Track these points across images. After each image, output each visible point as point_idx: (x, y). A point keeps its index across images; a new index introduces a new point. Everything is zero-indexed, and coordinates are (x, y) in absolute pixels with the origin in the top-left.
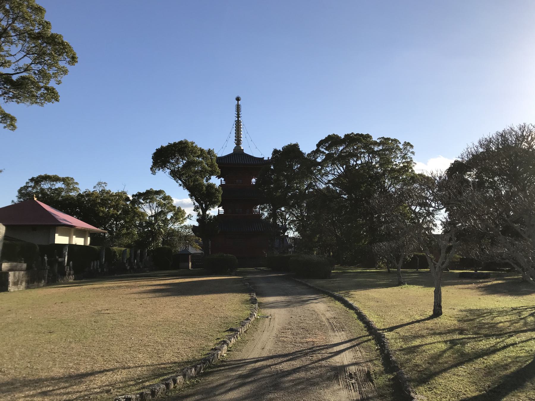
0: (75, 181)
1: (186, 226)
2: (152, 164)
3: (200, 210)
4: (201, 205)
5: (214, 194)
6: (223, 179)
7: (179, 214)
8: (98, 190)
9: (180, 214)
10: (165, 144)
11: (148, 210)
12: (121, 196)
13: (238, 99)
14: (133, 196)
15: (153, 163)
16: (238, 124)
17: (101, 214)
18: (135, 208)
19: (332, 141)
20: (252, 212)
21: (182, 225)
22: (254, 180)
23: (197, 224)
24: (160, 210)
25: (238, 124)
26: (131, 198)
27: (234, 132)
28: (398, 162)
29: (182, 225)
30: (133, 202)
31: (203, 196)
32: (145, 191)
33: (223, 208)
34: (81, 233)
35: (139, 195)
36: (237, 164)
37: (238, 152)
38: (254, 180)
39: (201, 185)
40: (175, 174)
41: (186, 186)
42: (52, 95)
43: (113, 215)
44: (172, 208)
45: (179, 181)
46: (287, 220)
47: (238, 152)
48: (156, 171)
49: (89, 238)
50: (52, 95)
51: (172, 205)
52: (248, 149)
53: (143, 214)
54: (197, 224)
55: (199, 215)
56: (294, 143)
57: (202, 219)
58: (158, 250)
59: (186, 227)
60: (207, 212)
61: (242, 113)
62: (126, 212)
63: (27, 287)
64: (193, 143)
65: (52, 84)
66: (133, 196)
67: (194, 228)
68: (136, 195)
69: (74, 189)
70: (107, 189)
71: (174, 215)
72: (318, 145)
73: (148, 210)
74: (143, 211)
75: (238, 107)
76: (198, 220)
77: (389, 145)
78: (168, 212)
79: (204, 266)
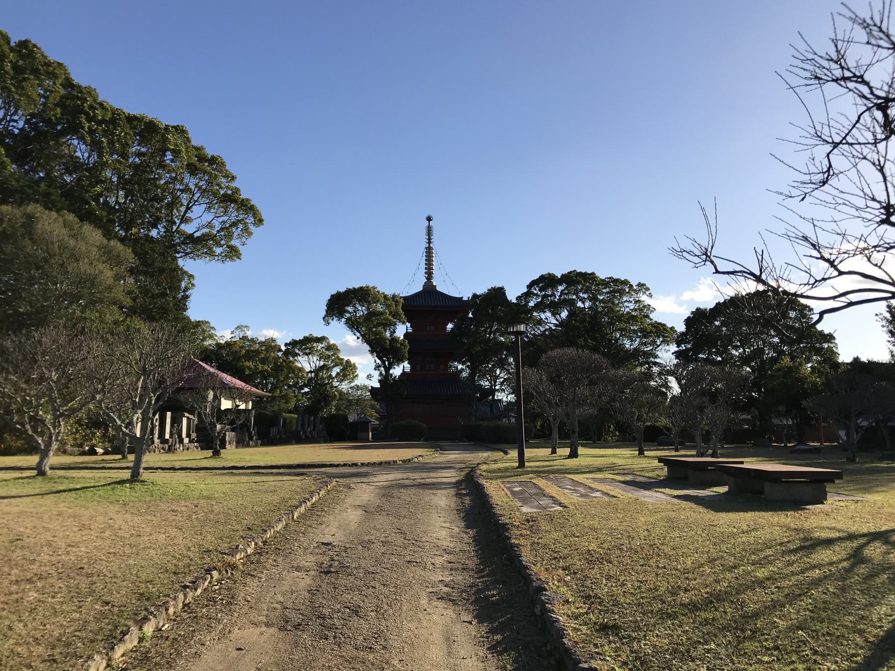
0: (211, 325)
1: (358, 386)
2: (325, 313)
3: (382, 369)
4: (383, 362)
5: (399, 349)
6: (408, 325)
7: (348, 370)
8: (238, 335)
9: (349, 369)
10: (342, 290)
11: (306, 363)
12: (270, 345)
13: (429, 219)
14: (286, 345)
15: (327, 311)
16: (429, 252)
17: (247, 372)
18: (291, 362)
19: (547, 281)
20: (447, 367)
21: (353, 384)
22: (450, 326)
23: (377, 385)
24: (322, 363)
25: (429, 252)
26: (283, 348)
27: (423, 266)
28: (628, 306)
29: (353, 384)
30: (287, 353)
31: (386, 352)
32: (302, 338)
33: (409, 363)
34: (242, 395)
35: (294, 343)
36: (428, 306)
37: (429, 290)
38: (450, 326)
39: (385, 339)
40: (353, 324)
41: (366, 339)
42: (233, 253)
43: (261, 372)
44: (339, 362)
45: (358, 334)
46: (497, 377)
47: (429, 290)
48: (330, 321)
49: (250, 403)
50: (233, 253)
51: (338, 357)
52: (445, 285)
53: (301, 370)
54: (377, 385)
55: (381, 374)
56: (499, 285)
57: (385, 379)
58: (332, 417)
59: (358, 388)
60: (391, 372)
61: (434, 238)
62: (277, 368)
63: (237, 447)
64: (374, 288)
65: (234, 242)
66: (286, 345)
67: (373, 390)
68: (290, 344)
69: (211, 337)
70: (250, 334)
71: (342, 370)
72: (530, 286)
73: (306, 363)
74: (300, 366)
75: (429, 230)
76: (380, 381)
77: (618, 286)
78: (334, 367)
79: (391, 433)
